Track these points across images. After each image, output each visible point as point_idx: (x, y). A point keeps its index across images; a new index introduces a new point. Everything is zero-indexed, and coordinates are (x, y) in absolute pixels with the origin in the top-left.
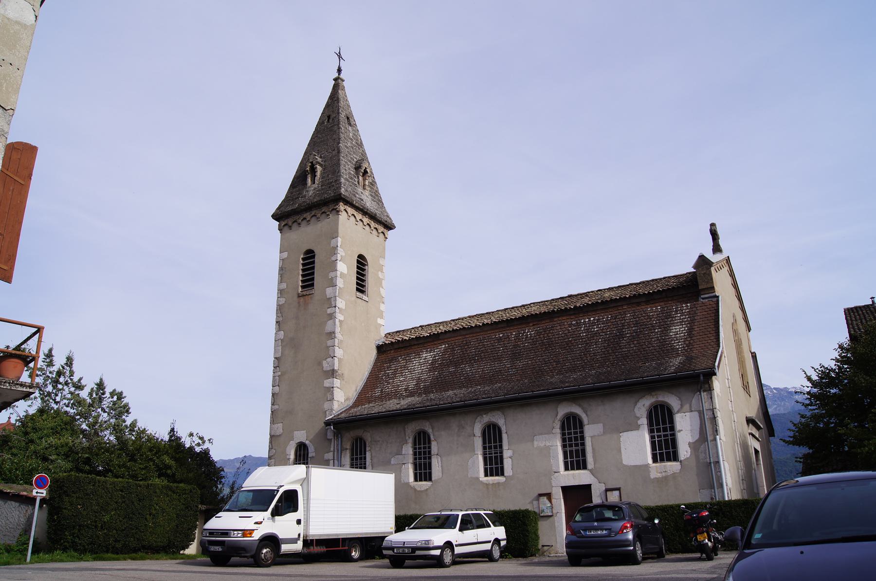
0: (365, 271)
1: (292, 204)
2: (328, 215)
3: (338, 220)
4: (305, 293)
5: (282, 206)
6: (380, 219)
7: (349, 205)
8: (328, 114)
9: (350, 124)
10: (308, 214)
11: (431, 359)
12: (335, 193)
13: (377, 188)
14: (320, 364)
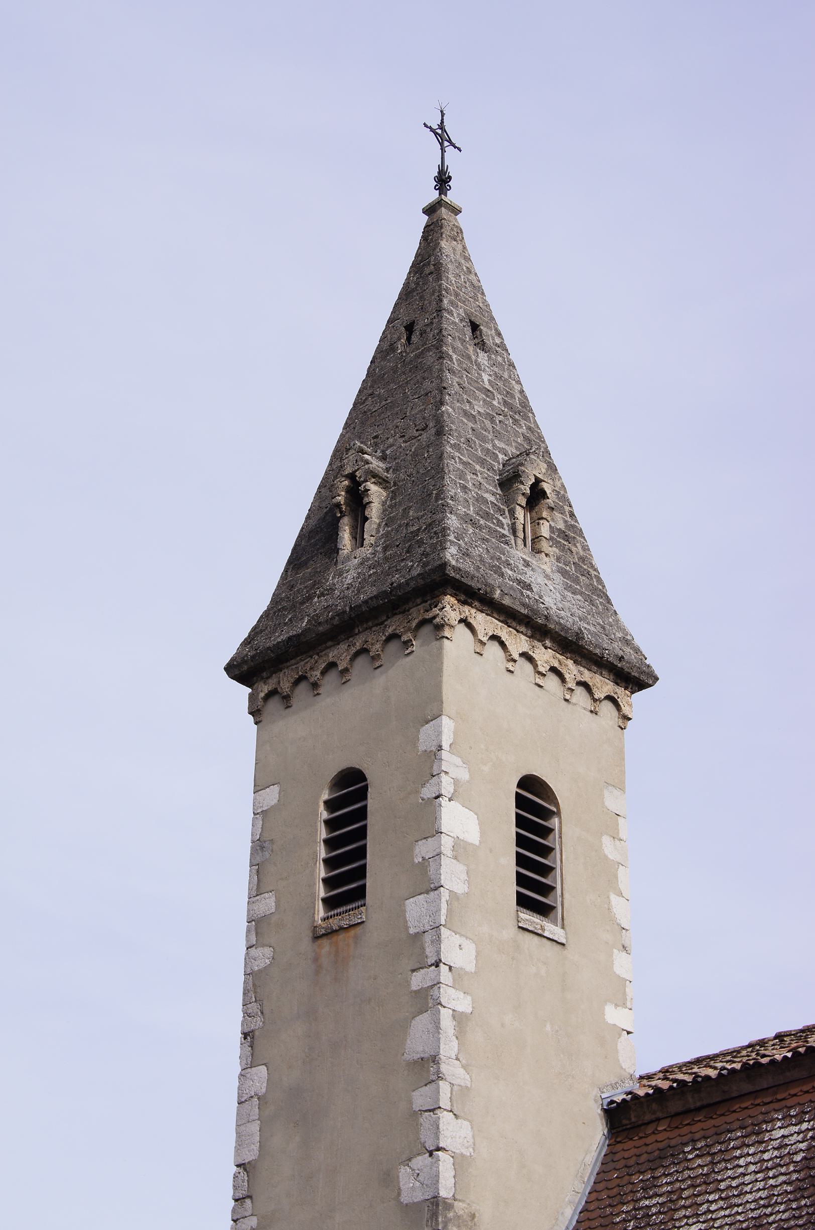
0: (551, 837)
1: (290, 620)
2: (408, 644)
3: (438, 657)
4: (335, 923)
5: (261, 631)
6: (598, 651)
7: (476, 603)
8: (406, 319)
9: (482, 345)
10: (343, 646)
11: (803, 1146)
12: (425, 565)
13: (586, 548)
14: (389, 1179)
